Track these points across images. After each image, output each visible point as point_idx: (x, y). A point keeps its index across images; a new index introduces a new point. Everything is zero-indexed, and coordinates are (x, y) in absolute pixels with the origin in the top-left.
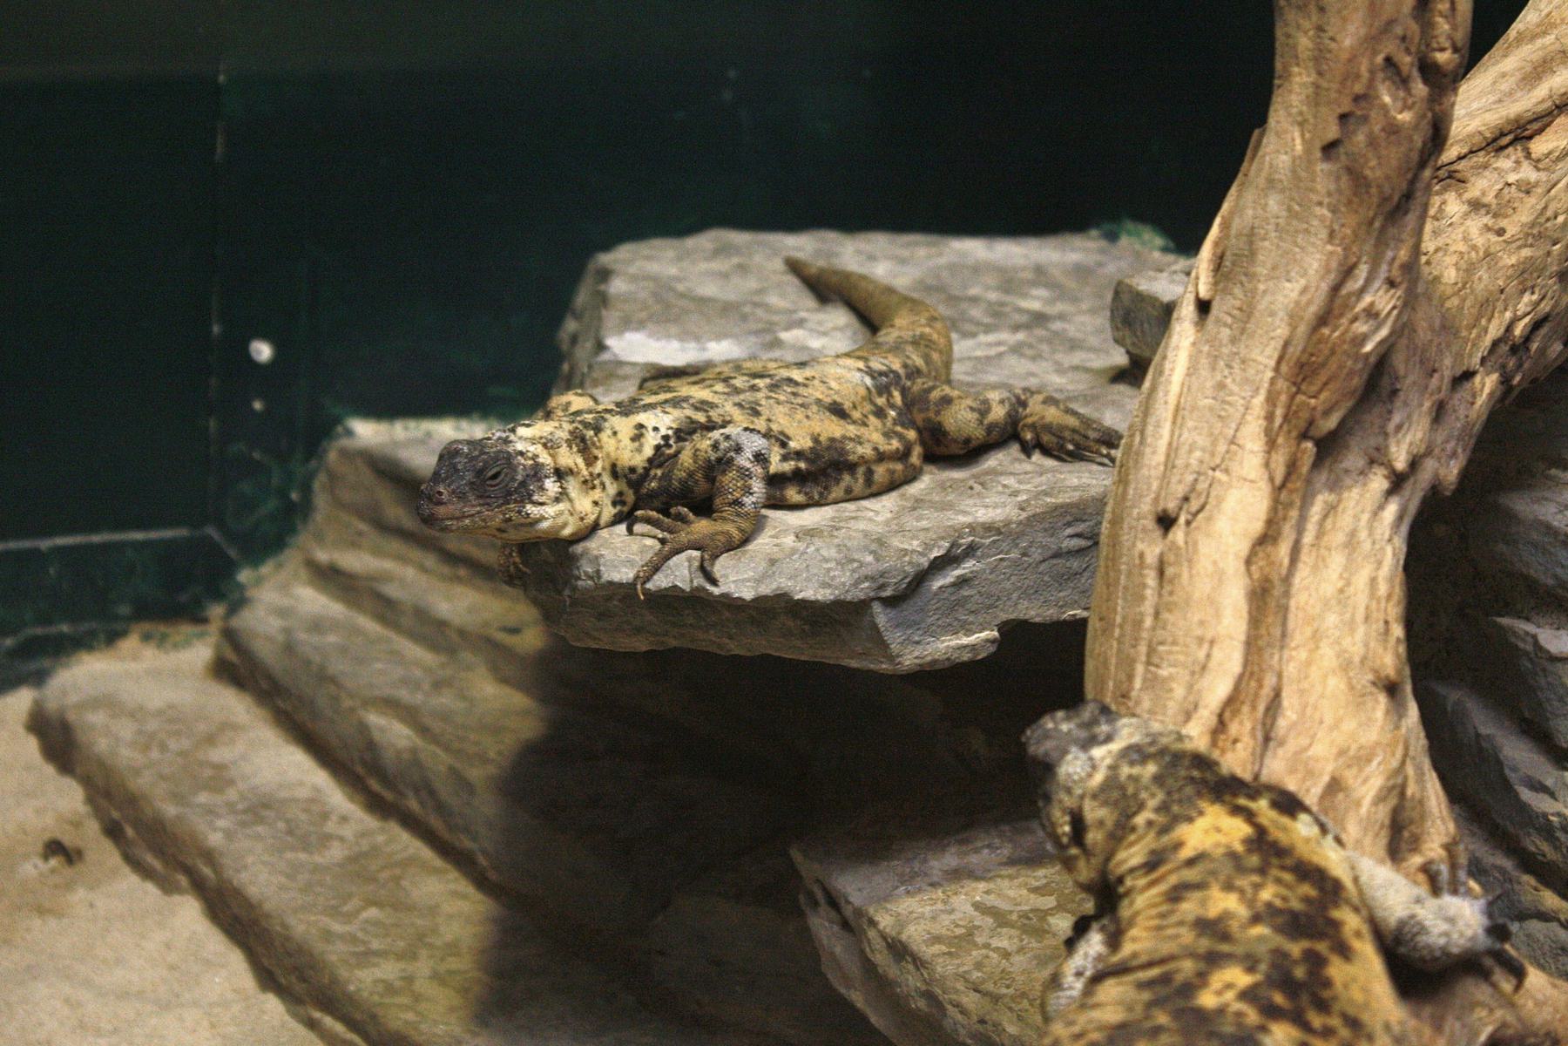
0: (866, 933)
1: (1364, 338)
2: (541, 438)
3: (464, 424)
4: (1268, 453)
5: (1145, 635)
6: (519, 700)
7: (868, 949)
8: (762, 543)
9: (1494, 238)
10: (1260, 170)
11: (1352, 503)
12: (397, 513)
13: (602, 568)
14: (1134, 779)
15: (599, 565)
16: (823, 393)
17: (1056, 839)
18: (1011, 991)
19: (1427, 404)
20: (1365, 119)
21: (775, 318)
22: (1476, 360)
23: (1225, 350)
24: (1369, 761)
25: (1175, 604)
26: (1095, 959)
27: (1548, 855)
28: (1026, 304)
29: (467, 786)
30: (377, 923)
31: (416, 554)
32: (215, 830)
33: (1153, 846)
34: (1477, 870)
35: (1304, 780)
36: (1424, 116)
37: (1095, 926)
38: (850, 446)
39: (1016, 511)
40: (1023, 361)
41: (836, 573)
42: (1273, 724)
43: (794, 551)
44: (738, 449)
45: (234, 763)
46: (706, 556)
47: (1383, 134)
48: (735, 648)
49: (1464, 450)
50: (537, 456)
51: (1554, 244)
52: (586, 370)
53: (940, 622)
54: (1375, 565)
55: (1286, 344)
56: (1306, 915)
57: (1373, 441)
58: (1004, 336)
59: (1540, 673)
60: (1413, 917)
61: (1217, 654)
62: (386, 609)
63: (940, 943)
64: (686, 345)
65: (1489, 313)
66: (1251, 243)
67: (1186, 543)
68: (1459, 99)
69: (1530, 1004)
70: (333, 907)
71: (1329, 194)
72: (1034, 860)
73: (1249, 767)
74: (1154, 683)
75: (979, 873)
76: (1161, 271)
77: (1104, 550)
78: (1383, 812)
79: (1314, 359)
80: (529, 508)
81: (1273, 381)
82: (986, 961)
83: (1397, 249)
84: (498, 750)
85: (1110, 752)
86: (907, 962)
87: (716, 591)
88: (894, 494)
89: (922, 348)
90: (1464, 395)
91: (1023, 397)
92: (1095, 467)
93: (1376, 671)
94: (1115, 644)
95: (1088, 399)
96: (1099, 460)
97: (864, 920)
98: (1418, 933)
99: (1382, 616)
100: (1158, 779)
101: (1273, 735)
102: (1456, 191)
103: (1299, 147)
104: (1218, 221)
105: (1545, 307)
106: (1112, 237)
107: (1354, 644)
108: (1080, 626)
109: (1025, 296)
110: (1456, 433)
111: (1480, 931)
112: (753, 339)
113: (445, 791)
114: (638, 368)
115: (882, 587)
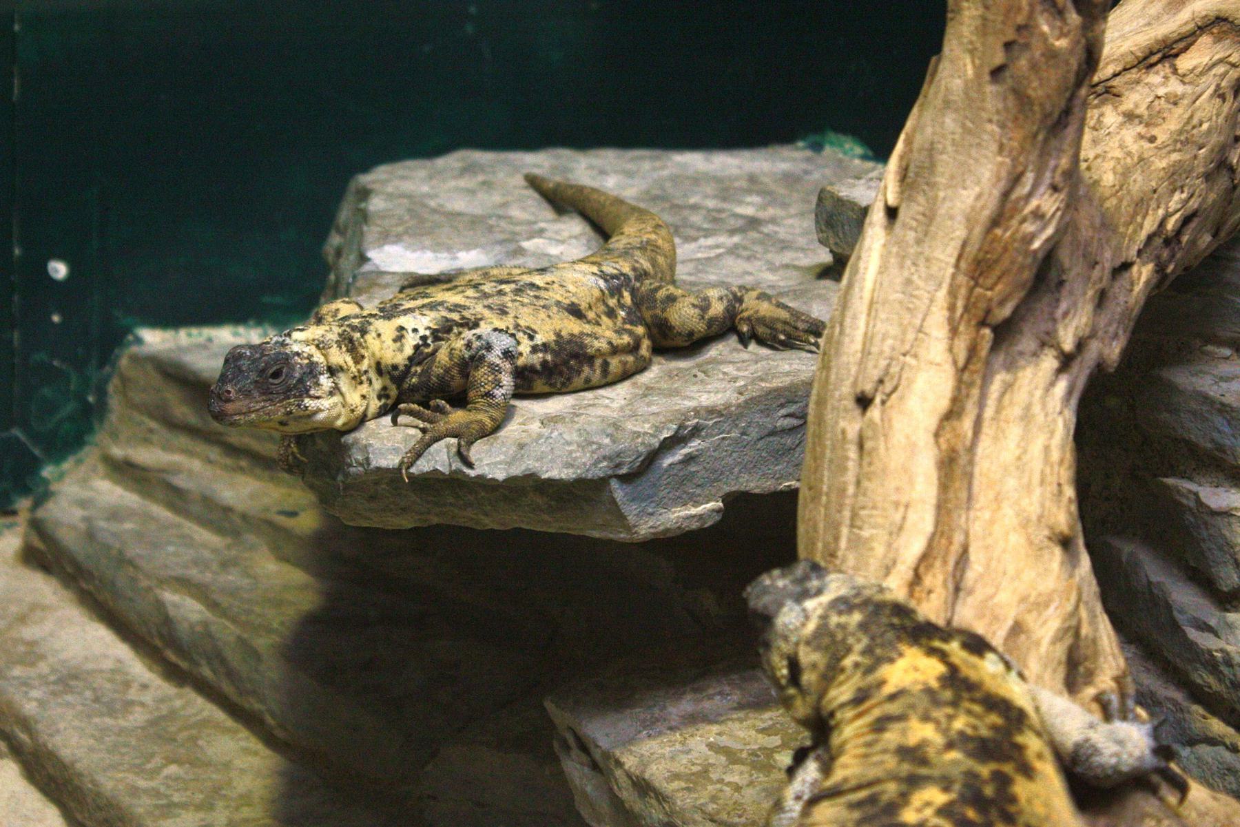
0: (613, 774)
1: (1032, 237)
2: (314, 340)
3: (241, 330)
4: (952, 339)
5: (848, 501)
6: (298, 576)
7: (615, 787)
8: (512, 430)
9: (1147, 145)
10: (936, 93)
11: (1027, 381)
12: (183, 411)
13: (371, 456)
14: (842, 627)
15: (368, 453)
16: (562, 295)
17: (775, 681)
18: (743, 820)
19: (1090, 293)
20: (1027, 46)
21: (518, 229)
22: (1133, 252)
23: (912, 251)
24: (1047, 605)
25: (874, 473)
26: (812, 784)
27: (1214, 687)
28: (741, 210)
29: (255, 655)
30: (177, 779)
31: (201, 447)
32: (30, 700)
33: (862, 684)
34: (1146, 699)
35: (990, 624)
36: (1078, 42)
37: (812, 755)
38: (588, 341)
39: (736, 395)
40: (739, 261)
41: (578, 454)
42: (962, 576)
43: (540, 436)
44: (489, 347)
45: (44, 639)
46: (463, 443)
47: (1043, 59)
48: (490, 523)
49: (1125, 332)
50: (312, 356)
51: (1200, 148)
52: (351, 280)
53: (671, 495)
54: (1049, 435)
55: (964, 244)
56: (994, 741)
57: (1044, 327)
58: (723, 239)
59: (1202, 526)
60: (1087, 740)
61: (912, 516)
62: (176, 498)
63: (679, 779)
64: (439, 255)
65: (1144, 211)
66: (931, 157)
67: (882, 420)
68: (1109, 24)
69: (1194, 815)
70: (135, 766)
71: (998, 112)
72: (759, 705)
73: (942, 615)
74: (857, 543)
75: (712, 717)
76: (859, 178)
77: (811, 428)
78: (1060, 651)
79: (989, 256)
80: (307, 401)
81: (954, 276)
82: (720, 794)
83: (1058, 158)
84: (281, 620)
85: (820, 604)
86: (650, 797)
87: (472, 473)
88: (627, 384)
89: (649, 253)
90: (1125, 284)
91: (739, 294)
92: (804, 354)
93: (1051, 528)
94: (822, 510)
95: (796, 294)
96: (808, 347)
97: (612, 762)
98: (1091, 755)
99: (1054, 479)
100: (863, 626)
101: (962, 585)
102: (1113, 104)
103: (970, 72)
104: (902, 137)
105: (1194, 204)
106: (817, 147)
107: (1031, 504)
108: (793, 494)
109: (740, 203)
110: (1117, 317)
111: (1147, 752)
112: (498, 248)
113: (235, 659)
114: (397, 278)
115: (618, 466)
